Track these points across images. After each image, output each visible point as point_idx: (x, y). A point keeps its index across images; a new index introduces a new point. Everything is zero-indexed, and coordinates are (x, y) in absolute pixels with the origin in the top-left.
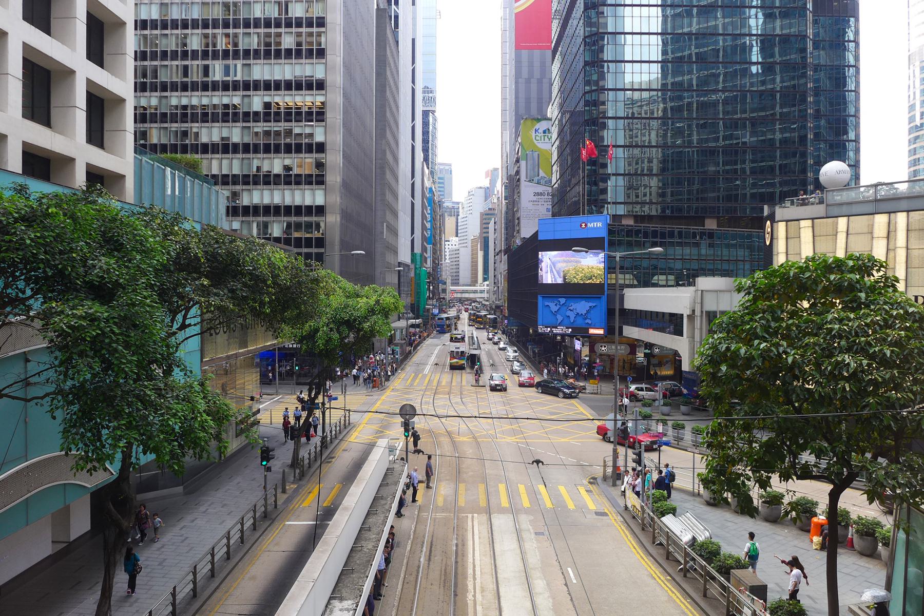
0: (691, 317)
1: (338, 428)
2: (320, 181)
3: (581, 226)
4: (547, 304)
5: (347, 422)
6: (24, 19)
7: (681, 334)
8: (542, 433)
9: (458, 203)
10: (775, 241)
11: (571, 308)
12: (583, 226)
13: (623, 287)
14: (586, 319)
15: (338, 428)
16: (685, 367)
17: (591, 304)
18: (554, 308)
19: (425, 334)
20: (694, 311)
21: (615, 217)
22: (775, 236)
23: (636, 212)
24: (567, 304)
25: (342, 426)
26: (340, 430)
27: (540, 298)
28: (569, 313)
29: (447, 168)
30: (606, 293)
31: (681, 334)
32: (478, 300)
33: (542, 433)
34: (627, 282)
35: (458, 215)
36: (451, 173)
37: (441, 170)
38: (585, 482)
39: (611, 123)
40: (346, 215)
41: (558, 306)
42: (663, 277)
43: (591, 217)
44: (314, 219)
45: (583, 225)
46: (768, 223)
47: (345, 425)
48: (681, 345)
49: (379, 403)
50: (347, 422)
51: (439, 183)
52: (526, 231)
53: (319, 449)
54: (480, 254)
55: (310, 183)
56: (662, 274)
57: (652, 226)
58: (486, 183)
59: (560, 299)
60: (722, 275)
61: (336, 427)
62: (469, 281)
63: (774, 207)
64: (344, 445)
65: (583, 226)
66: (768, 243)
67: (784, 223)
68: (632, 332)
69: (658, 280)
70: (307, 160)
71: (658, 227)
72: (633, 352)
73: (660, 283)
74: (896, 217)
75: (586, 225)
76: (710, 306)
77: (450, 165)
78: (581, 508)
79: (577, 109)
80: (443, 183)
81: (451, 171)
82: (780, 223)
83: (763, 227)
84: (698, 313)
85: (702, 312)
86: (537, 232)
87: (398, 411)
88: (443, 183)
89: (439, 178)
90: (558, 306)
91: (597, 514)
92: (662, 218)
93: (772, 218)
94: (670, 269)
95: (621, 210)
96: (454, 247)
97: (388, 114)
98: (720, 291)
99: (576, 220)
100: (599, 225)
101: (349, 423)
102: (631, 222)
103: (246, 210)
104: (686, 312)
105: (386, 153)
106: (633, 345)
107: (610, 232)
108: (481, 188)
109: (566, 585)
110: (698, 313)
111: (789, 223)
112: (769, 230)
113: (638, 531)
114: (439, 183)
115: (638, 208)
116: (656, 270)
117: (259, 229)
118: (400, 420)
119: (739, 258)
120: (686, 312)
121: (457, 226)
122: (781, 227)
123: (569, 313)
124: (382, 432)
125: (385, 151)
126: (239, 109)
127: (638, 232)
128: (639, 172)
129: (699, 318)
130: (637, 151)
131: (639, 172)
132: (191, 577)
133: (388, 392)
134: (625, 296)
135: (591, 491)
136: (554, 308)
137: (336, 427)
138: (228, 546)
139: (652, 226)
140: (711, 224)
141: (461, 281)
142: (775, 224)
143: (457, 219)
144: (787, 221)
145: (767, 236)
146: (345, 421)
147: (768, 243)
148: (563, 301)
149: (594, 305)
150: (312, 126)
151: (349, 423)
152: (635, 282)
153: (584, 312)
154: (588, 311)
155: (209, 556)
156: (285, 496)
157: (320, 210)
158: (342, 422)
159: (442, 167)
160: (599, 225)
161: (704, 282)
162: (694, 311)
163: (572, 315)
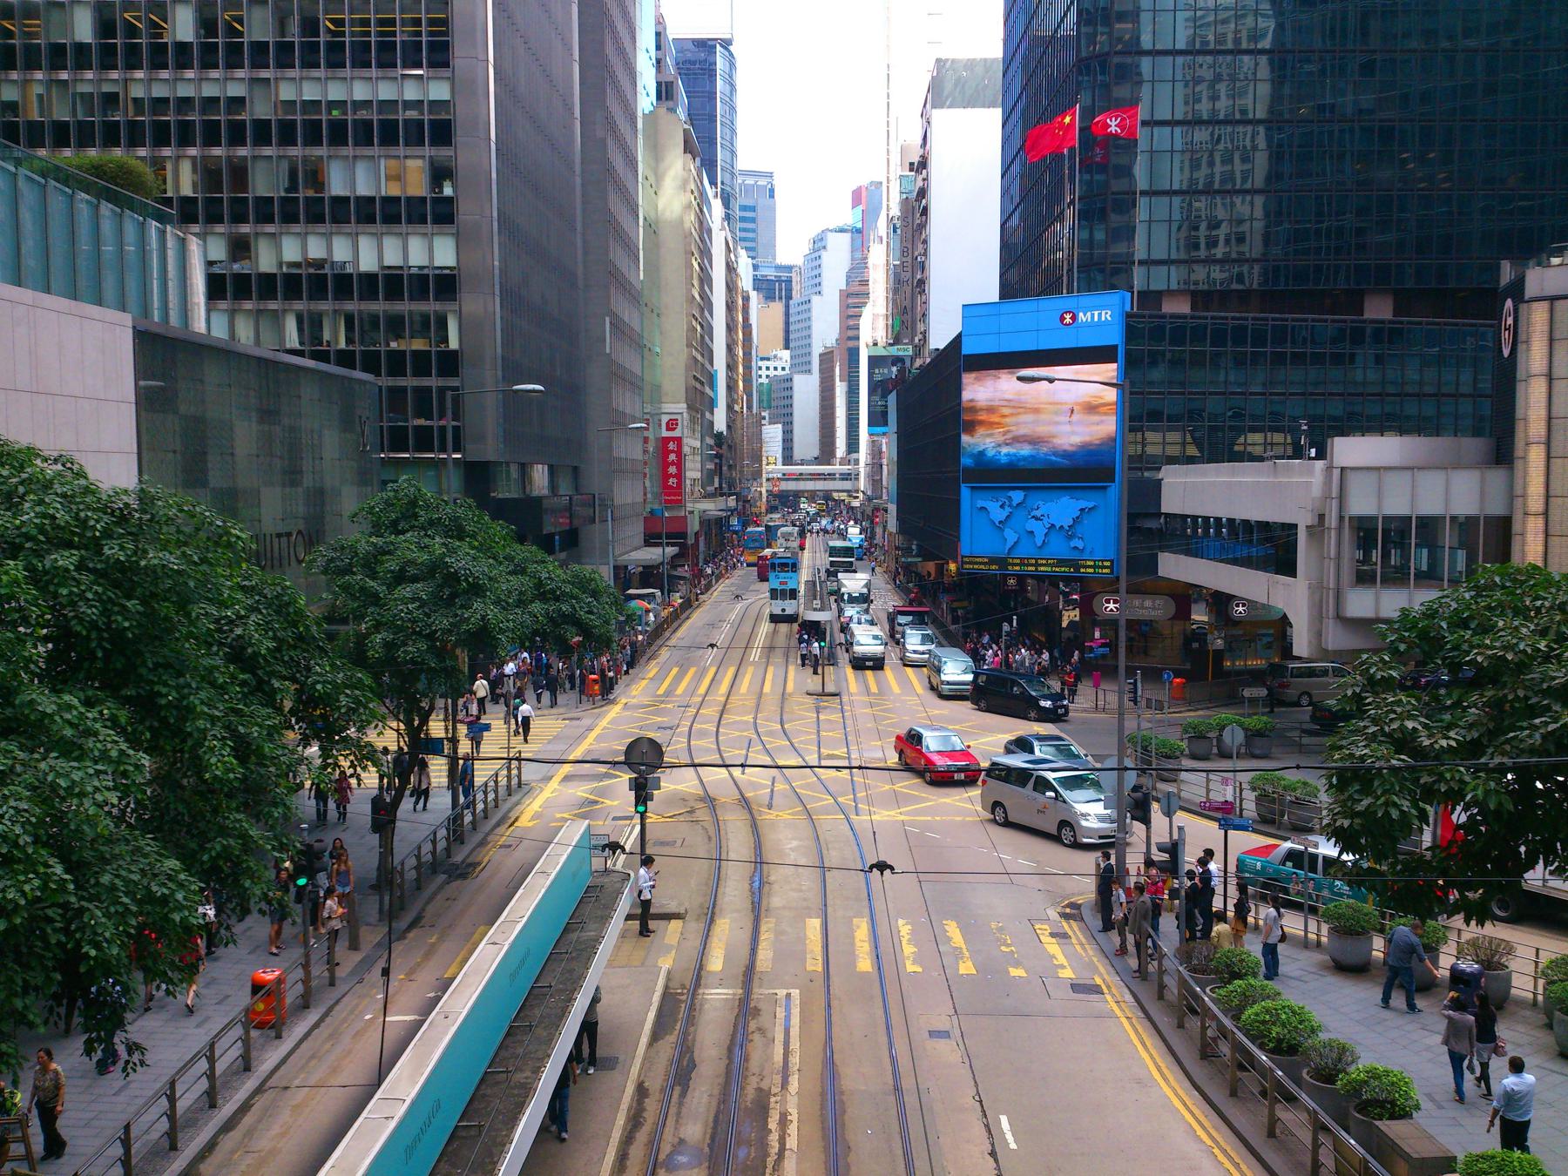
0: (1318, 529)
1: (491, 796)
2: (441, 214)
3: (1062, 319)
4: (980, 503)
5: (515, 781)
9: (789, 268)
10: (1521, 347)
11: (1038, 513)
13: (1156, 463)
14: (1070, 537)
15: (491, 796)
16: (1301, 645)
18: (998, 514)
20: (1321, 517)
21: (1149, 298)
22: (1522, 337)
23: (1197, 283)
24: (1030, 502)
25: (502, 791)
26: (496, 800)
27: (965, 492)
28: (1032, 525)
29: (762, 182)
32: (835, 495)
34: (1174, 450)
35: (789, 297)
36: (772, 196)
37: (749, 190)
38: (1053, 914)
39: (1146, 64)
40: (513, 299)
41: (1008, 510)
42: (1257, 438)
43: (1087, 299)
44: (431, 306)
46: (1509, 303)
47: (509, 786)
49: (592, 736)
50: (515, 781)
51: (743, 219)
52: (939, 338)
53: (442, 845)
54: (840, 389)
55: (371, 220)
56: (1254, 430)
57: (1231, 317)
58: (851, 217)
59: (1011, 493)
60: (1402, 431)
61: (485, 793)
63: (1526, 266)
64: (505, 835)
66: (1506, 353)
67: (1545, 305)
68: (1174, 566)
69: (1245, 444)
70: (410, 163)
71: (1250, 317)
72: (1183, 613)
73: (1258, 450)
74: (1529, 308)
76: (1361, 504)
77: (770, 175)
78: (1045, 974)
79: (1061, 33)
80: (753, 220)
81: (772, 191)
82: (1535, 305)
83: (1497, 314)
84: (1332, 521)
85: (1341, 518)
86: (959, 336)
87: (622, 758)
88: (753, 220)
89: (744, 208)
90: (1008, 510)
91: (1076, 988)
92: (1269, 298)
93: (1517, 290)
94: (1275, 415)
95: (1160, 279)
96: (780, 372)
97: (610, 50)
98: (1386, 468)
99: (1051, 306)
101: (520, 785)
102: (1182, 307)
103: (267, 285)
104: (1303, 520)
105: (605, 145)
106: (1184, 595)
108: (842, 230)
109: (993, 1154)
110: (1332, 521)
111: (1559, 304)
112: (1510, 321)
113: (1165, 1022)
114: (743, 219)
115: (1200, 273)
116: (1242, 421)
117: (300, 330)
118: (625, 777)
119: (1444, 390)
120: (1303, 520)
121: (787, 324)
122: (1538, 316)
123: (1032, 525)
124: (596, 802)
125: (603, 142)
126: (241, 34)
127: (1198, 334)
128: (1216, 186)
129: (1333, 533)
130: (1201, 135)
131: (1216, 186)
132: (118, 1150)
133: (614, 711)
135: (1065, 936)
136: (998, 514)
137: (485, 793)
138: (211, 1075)
139: (1231, 317)
140: (1379, 309)
141: (798, 453)
142: (1523, 307)
143: (787, 307)
144: (1553, 299)
145: (1505, 335)
146: (509, 777)
147: (1506, 353)
148: (1017, 496)
149: (1091, 505)
150: (421, 76)
151: (520, 785)
152: (1192, 451)
153: (1067, 522)
155: (164, 1102)
156: (357, 957)
157: (446, 284)
158: (503, 781)
159: (750, 181)
160: (1107, 315)
161: (1350, 450)
162: (1321, 517)
163: (1039, 529)
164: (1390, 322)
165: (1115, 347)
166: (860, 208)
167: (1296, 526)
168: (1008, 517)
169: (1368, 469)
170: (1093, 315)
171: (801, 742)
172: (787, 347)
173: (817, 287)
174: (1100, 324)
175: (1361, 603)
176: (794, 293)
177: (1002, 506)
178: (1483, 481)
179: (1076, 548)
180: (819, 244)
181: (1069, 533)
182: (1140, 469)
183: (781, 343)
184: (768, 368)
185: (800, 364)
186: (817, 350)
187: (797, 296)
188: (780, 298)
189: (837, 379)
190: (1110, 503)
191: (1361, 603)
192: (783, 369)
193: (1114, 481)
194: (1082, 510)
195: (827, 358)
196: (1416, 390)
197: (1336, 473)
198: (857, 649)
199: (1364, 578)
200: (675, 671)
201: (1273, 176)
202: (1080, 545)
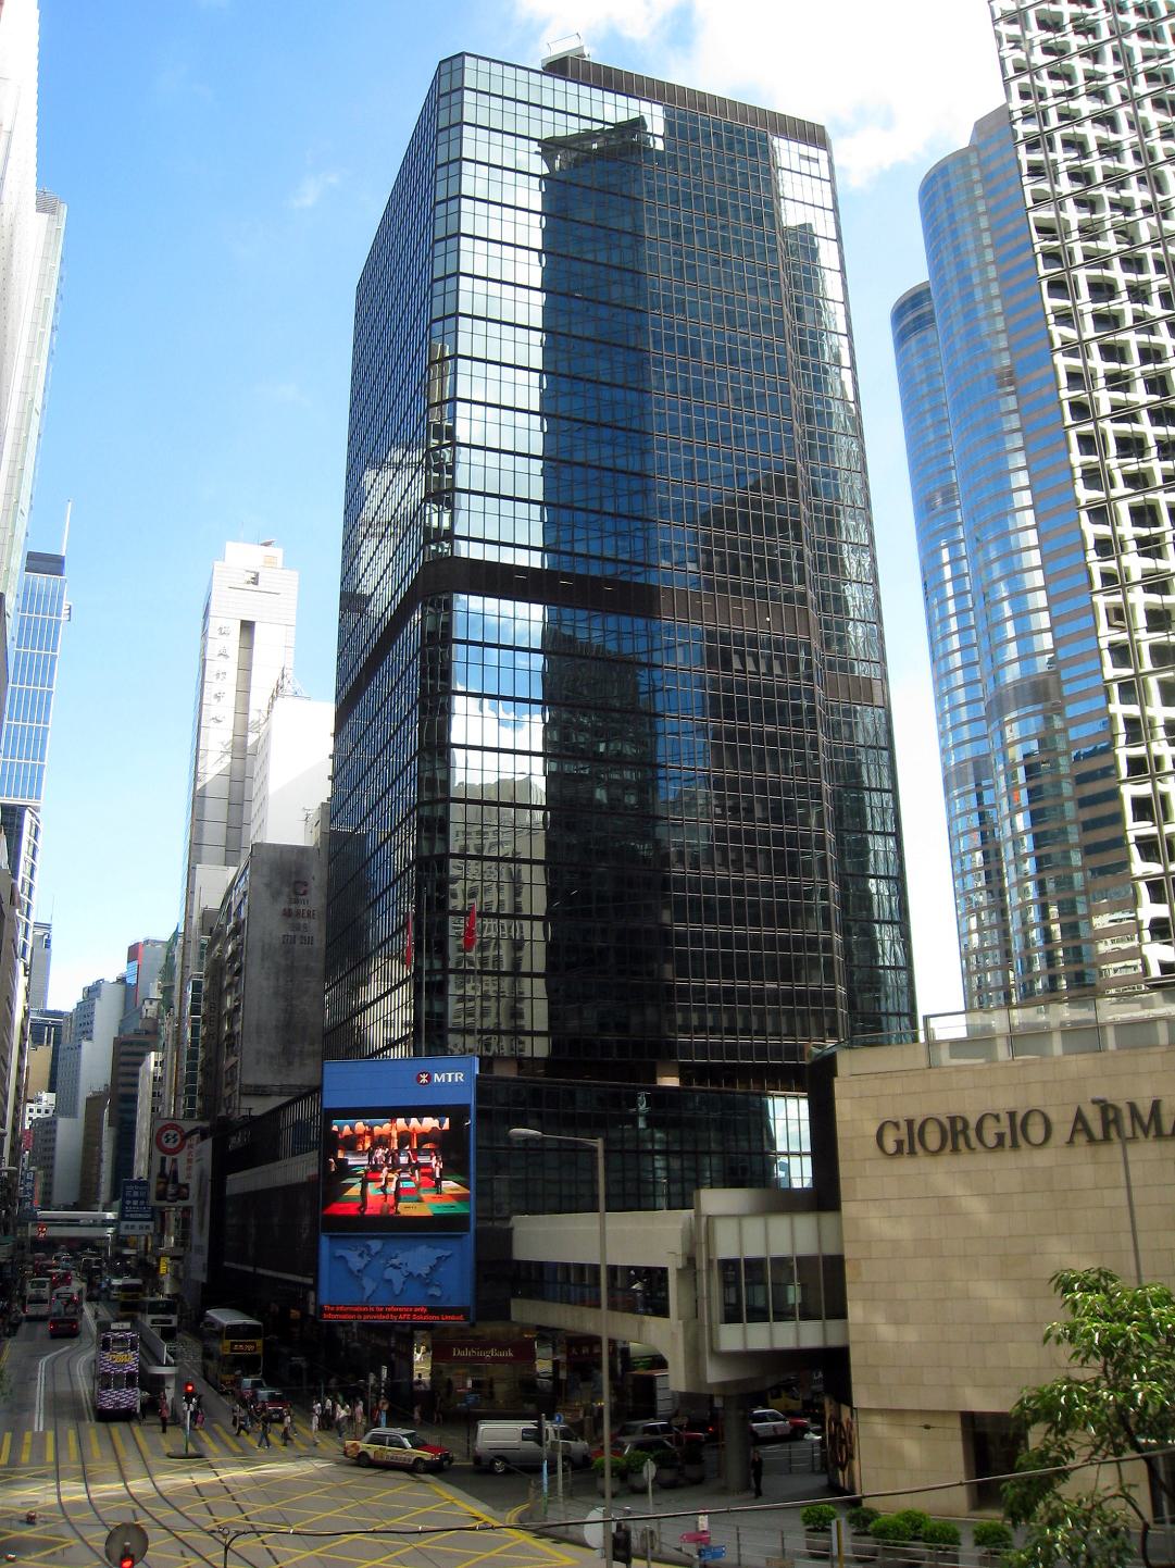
3: (419, 1079)
4: (340, 1252)
6: (976, 123)
7: (662, 1311)
8: (340, 1513)
12: (424, 1080)
17: (439, 1253)
19: (499, 1434)
27: (324, 1241)
28: (390, 1273)
30: (472, 1227)
31: (662, 1311)
33: (340, 1513)
36: (48, 946)
41: (367, 1259)
45: (424, 1076)
48: (660, 1335)
59: (370, 1242)
62: (72, 1198)
65: (424, 1080)
68: (526, 1312)
75: (429, 1078)
76: (726, 1248)
77: (48, 927)
81: (48, 941)
85: (710, 1262)
90: (367, 1259)
100: (459, 1077)
104: (672, 1263)
107: (482, 1093)
120: (672, 1263)
134: (516, 1235)
136: (356, 1262)
141: (57, 1198)
148: (376, 1245)
149: (448, 1253)
153: (424, 1270)
154: (433, 1268)
160: (459, 1077)
164: (514, 1080)
165: (467, 1107)
166: (136, 963)
167: (664, 1270)
168: (366, 1265)
169: (734, 1216)
170: (447, 1077)
171: (92, 1540)
172: (51, 1090)
173: (87, 1033)
174: (454, 1084)
175: (732, 1338)
176: (63, 1037)
177: (361, 1255)
178: (818, 1224)
179: (432, 1296)
180: (92, 992)
181: (426, 1281)
182: (491, 1219)
183: (46, 1085)
184: (39, 1111)
185: (64, 1108)
186: (84, 1093)
187: (66, 1041)
188: (48, 1042)
189: (105, 1124)
190: (459, 1256)
191: (732, 1338)
192: (31, 1111)
193: (468, 1230)
194: (439, 1258)
195: (94, 1102)
196: (619, 1147)
197: (704, 1220)
198: (159, 1420)
199: (732, 1316)
200: (8, 1435)
201: (550, 964)
202: (437, 1292)
